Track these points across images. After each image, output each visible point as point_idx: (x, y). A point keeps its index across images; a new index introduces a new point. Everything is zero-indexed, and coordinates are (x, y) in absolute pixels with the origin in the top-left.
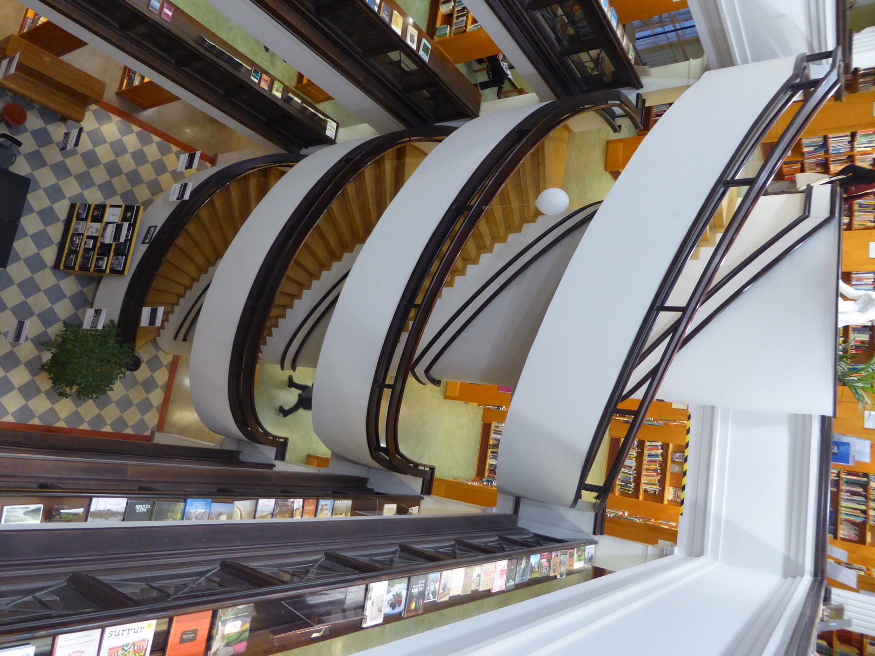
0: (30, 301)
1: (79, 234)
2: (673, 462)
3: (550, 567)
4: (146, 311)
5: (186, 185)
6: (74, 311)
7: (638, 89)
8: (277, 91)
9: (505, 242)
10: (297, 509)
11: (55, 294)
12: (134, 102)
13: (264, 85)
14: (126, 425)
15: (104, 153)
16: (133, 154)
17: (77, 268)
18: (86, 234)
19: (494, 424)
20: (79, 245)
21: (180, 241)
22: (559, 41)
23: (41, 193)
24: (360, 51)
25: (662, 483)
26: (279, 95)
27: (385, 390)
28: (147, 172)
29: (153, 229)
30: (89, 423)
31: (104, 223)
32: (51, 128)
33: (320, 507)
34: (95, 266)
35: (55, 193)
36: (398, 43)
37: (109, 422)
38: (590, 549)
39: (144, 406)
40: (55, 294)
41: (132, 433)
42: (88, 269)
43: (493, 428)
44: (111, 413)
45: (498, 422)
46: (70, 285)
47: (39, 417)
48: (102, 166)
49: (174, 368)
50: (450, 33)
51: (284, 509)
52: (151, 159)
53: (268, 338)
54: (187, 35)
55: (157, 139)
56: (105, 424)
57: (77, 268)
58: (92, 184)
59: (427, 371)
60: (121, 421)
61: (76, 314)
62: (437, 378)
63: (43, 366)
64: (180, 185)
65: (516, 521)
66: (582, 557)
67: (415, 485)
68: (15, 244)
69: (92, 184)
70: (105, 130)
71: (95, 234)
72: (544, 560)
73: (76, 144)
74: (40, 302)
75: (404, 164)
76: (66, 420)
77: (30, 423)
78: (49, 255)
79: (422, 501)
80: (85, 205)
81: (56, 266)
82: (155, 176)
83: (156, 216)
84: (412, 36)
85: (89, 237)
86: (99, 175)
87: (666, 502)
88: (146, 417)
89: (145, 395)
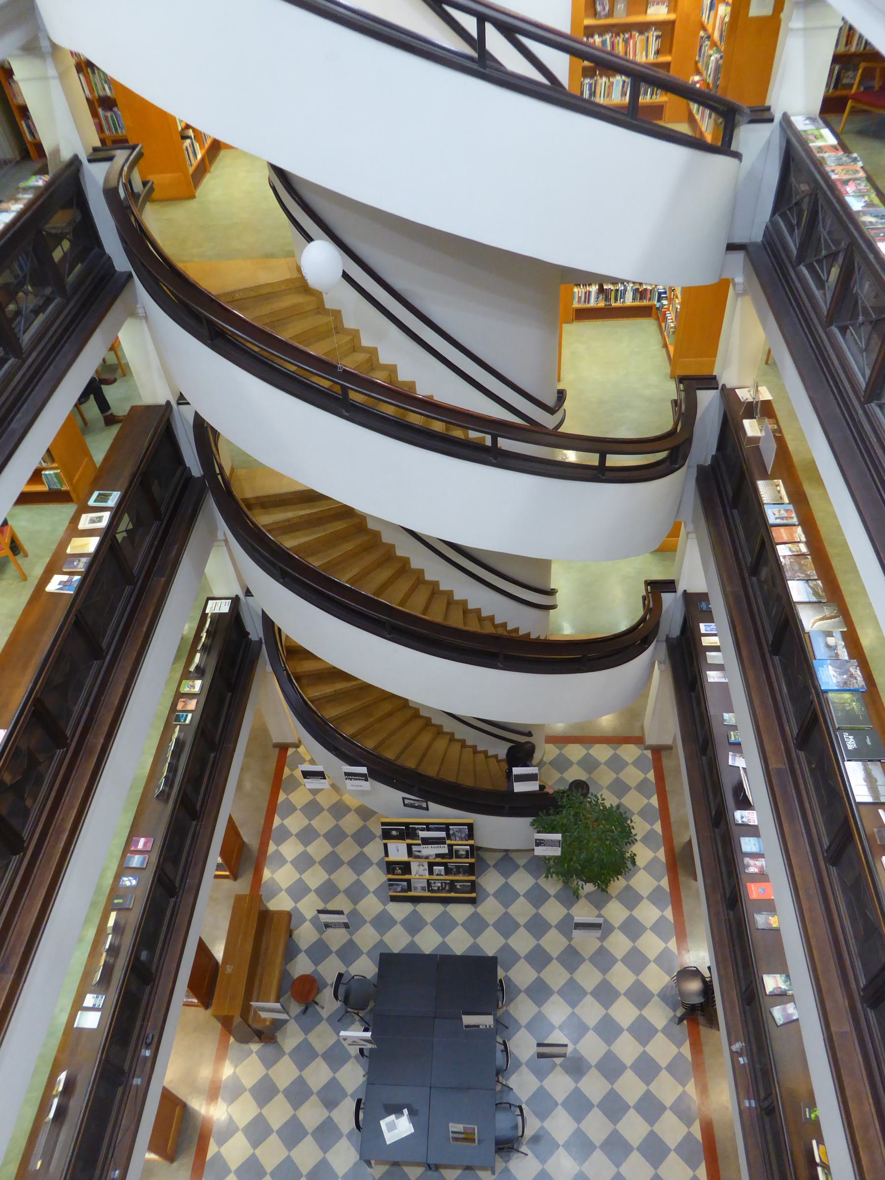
0: (522, 921)
1: (429, 884)
2: (610, 14)
3: (854, 180)
4: (519, 787)
5: (346, 774)
6: (521, 869)
7: (80, 163)
8: (193, 687)
9: (358, 331)
10: (790, 550)
11: (506, 895)
12: (242, 859)
13: (192, 704)
14: (645, 781)
15: (315, 878)
16: (306, 844)
17: (472, 878)
18: (427, 876)
19: (576, 305)
20: (443, 882)
21: (411, 764)
22: (48, 300)
23: (388, 938)
24: (128, 589)
25: (643, 28)
26: (198, 683)
27: (608, 464)
28: (323, 823)
29: (407, 802)
30: (652, 823)
31: (411, 859)
32: (303, 945)
33: (779, 521)
34: (467, 857)
35: (383, 922)
36: (108, 535)
37: (646, 801)
38: (801, 123)
39: (616, 764)
40: (506, 895)
41: (652, 772)
42: (472, 864)
43: (582, 305)
44: (634, 802)
45: (573, 299)
46: (491, 881)
47: (659, 881)
48: (332, 877)
49: (587, 740)
50: (51, 469)
51: (796, 567)
52: (306, 822)
53: (521, 633)
54: (162, 815)
55: (277, 821)
56: (649, 804)
57: (472, 878)
58: (358, 882)
59: (552, 411)
60: (641, 787)
61: (525, 867)
62: (555, 396)
63: (603, 890)
64: (348, 781)
65: (754, 244)
66: (816, 132)
67: (706, 398)
68: (459, 953)
69: (358, 882)
70: (285, 880)
71: (426, 867)
72: (848, 189)
73: (340, 913)
74: (521, 910)
75: (257, 498)
76: (655, 851)
77: (668, 890)
78: (460, 912)
79: (729, 386)
80: (390, 885)
81: (473, 901)
82: (325, 813)
83: (389, 801)
84: (92, 521)
85: (431, 872)
86: (344, 877)
87: (672, 17)
88: (629, 759)
89: (603, 767)
